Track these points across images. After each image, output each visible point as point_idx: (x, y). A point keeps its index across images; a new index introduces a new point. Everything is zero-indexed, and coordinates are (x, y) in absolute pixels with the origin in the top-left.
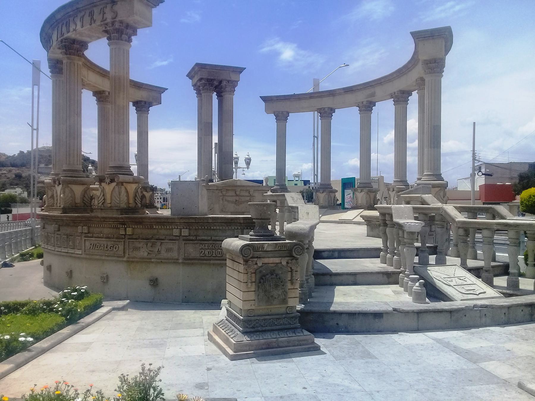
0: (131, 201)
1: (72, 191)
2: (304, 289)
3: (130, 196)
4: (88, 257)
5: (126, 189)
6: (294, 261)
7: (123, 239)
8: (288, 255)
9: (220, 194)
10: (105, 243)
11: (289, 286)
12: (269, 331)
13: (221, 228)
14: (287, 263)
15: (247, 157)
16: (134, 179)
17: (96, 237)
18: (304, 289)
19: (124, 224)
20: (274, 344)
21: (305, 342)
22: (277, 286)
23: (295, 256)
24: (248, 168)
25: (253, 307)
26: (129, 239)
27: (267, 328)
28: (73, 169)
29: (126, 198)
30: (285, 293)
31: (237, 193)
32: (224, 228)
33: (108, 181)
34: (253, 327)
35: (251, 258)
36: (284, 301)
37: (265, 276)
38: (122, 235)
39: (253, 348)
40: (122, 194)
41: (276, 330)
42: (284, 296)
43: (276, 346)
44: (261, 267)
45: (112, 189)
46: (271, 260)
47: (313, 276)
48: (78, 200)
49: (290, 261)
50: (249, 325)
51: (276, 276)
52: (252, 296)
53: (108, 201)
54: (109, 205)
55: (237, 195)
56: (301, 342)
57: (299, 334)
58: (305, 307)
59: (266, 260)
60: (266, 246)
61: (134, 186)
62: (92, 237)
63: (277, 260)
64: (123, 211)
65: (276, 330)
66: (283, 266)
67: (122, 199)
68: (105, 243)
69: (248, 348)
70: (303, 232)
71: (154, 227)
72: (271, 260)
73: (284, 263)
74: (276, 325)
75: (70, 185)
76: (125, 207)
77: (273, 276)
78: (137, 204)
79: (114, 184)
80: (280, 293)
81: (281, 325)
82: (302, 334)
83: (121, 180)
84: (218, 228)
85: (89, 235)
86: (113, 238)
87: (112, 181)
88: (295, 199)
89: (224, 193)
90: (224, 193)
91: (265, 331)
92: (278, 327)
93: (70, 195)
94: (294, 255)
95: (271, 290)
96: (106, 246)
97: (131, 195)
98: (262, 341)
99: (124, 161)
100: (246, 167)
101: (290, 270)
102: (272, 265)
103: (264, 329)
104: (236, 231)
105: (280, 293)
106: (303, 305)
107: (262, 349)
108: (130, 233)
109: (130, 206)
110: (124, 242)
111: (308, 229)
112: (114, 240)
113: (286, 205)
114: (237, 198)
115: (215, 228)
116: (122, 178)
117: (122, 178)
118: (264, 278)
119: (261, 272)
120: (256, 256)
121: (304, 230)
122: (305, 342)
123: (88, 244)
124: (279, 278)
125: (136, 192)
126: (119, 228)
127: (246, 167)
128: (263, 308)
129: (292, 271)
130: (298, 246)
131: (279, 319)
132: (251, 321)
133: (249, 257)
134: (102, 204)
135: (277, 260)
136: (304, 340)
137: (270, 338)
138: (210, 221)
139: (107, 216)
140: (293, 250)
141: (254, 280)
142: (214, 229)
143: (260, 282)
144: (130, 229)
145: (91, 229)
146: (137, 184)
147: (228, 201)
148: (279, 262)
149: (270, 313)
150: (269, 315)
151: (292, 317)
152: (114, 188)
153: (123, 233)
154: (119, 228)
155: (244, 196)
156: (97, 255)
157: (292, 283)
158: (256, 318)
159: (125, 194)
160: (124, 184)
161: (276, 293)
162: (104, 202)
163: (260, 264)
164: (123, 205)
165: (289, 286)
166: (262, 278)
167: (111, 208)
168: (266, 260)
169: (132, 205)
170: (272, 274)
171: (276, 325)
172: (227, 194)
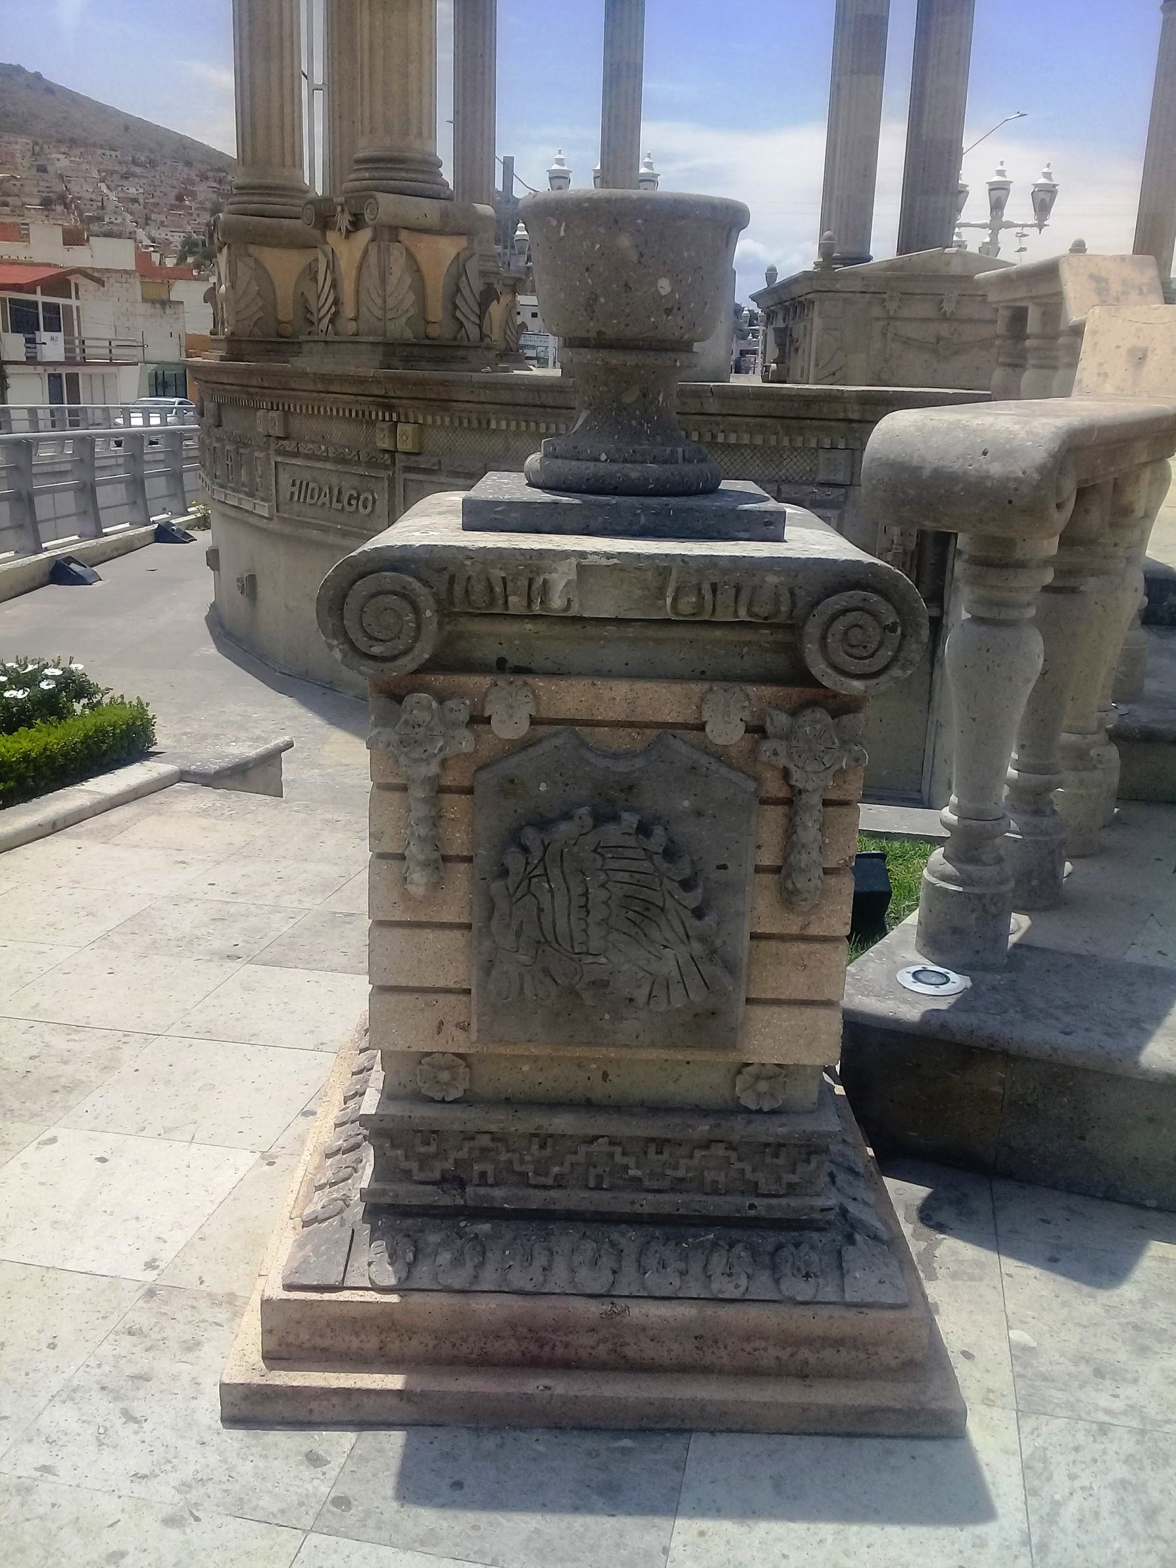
0: (437, 311)
1: (262, 273)
2: (988, 872)
3: (429, 283)
4: (287, 530)
5: (411, 256)
6: (816, 721)
7: (386, 467)
8: (778, 663)
9: (876, 311)
10: (334, 480)
11: (761, 909)
12: (571, 1217)
13: (759, 440)
14: (757, 730)
15: (1042, 181)
16: (445, 215)
17: (308, 457)
18: (988, 872)
19: (390, 408)
20: (586, 1340)
21: (845, 1356)
22: (642, 913)
23: (830, 679)
24: (1040, 226)
25: (460, 1043)
26: (408, 469)
27: (563, 1199)
28: (269, 181)
29: (412, 297)
30: (717, 961)
31: (945, 306)
32: (773, 440)
33: (344, 220)
34: (443, 1181)
35: (423, 669)
36: (709, 1024)
37: (543, 823)
38: (385, 451)
39: (415, 1346)
40: (393, 280)
41: (635, 1220)
42: (698, 996)
43: (602, 1351)
44: (525, 745)
45: (358, 254)
46: (617, 698)
47: (1113, 752)
48: (286, 311)
49: (782, 719)
50: (423, 1162)
51: (644, 829)
52: (445, 959)
53: (349, 311)
54: (352, 327)
55: (945, 318)
56: (805, 1353)
57: (803, 1290)
58: (965, 1001)
59: (570, 698)
60: (560, 578)
61: (449, 248)
62: (296, 455)
63: (665, 701)
64: (394, 351)
65: (635, 1220)
66: (720, 755)
67: (391, 302)
68: (334, 480)
69: (372, 1343)
70: (996, 469)
71: (493, 425)
72: (617, 698)
73: (726, 730)
74: (636, 1184)
75: (252, 249)
76: (409, 335)
77: (612, 833)
78: (462, 325)
79: (364, 236)
80: (668, 967)
81: (678, 1185)
82: (829, 1292)
83: (382, 216)
84: (746, 439)
85: (289, 445)
86: (358, 463)
87: (357, 223)
88: (1115, 287)
89: (892, 306)
90: (892, 306)
91: (544, 1217)
92: (647, 1203)
93: (255, 288)
94: (818, 668)
95: (595, 944)
96: (336, 492)
97: (436, 285)
98: (487, 1307)
99: (406, 133)
100: (1032, 221)
101: (774, 787)
102: (623, 740)
103: (536, 1199)
104: (822, 455)
105: (668, 967)
106: (958, 982)
107: (483, 1363)
108: (409, 447)
109: (434, 331)
110: (392, 481)
111: (1040, 455)
112: (361, 471)
113: (1062, 327)
114: (944, 329)
115: (733, 439)
116: (388, 206)
117: (388, 206)
118: (531, 837)
119: (510, 786)
120: (489, 651)
121: (1008, 453)
122: (845, 1356)
123: (285, 479)
124: (670, 853)
125: (459, 269)
126: (372, 423)
127: (1032, 221)
128: (533, 1057)
129: (791, 801)
130: (854, 597)
131: (661, 1144)
132: (433, 1134)
133: (408, 663)
134: (332, 321)
135: (665, 701)
136: (838, 1343)
137: (566, 1286)
138: (712, 406)
139: (340, 370)
140: (812, 629)
141: (458, 840)
142: (727, 446)
143: (504, 873)
144: (409, 428)
145: (297, 424)
146: (463, 242)
147: (907, 342)
148: (686, 715)
149: (599, 1091)
150: (588, 1105)
151: (778, 1147)
152: (366, 252)
153: (386, 444)
154: (372, 423)
155: (970, 321)
156: (310, 526)
157: (788, 898)
158: (472, 1118)
159: (408, 280)
160: (403, 235)
161: (629, 962)
162: (336, 313)
163: (510, 725)
164: (399, 328)
165: (761, 909)
166: (515, 839)
167: (354, 340)
168: (570, 698)
169: (441, 329)
170: (604, 816)
171: (636, 1184)
172: (905, 313)
